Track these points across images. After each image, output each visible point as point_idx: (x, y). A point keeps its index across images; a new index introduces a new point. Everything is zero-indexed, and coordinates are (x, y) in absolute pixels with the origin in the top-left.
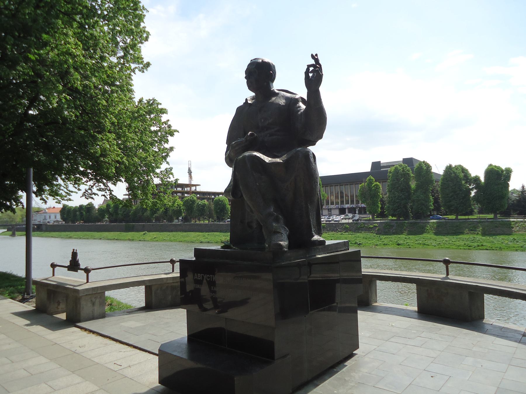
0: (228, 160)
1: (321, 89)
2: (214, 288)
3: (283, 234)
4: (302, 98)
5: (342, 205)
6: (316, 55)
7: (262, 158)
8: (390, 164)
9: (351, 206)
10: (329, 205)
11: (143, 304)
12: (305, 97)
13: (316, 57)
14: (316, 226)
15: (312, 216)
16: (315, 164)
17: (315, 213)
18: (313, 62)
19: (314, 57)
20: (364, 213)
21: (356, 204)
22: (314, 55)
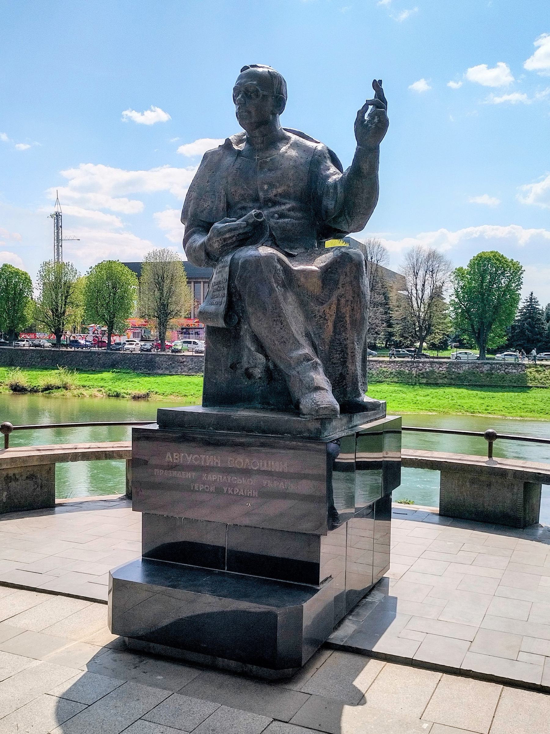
2: (207, 477)
6: (380, 81)
19: (377, 85)
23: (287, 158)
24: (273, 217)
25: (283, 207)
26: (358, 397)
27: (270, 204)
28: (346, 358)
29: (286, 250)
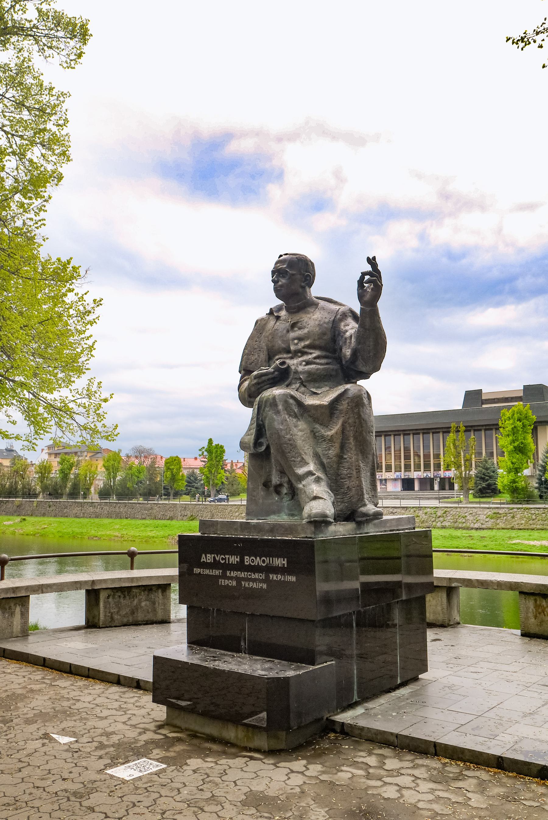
1: (379, 304)
2: (230, 573)
5: (407, 473)
6: (374, 258)
8: (507, 396)
9: (425, 475)
10: (401, 471)
11: (83, 623)
12: (358, 311)
16: (371, 407)
18: (369, 268)
19: (372, 261)
20: (450, 489)
21: (434, 470)
22: (371, 258)
24: (301, 364)
25: (310, 356)
26: (49, 472)
29: (312, 390)
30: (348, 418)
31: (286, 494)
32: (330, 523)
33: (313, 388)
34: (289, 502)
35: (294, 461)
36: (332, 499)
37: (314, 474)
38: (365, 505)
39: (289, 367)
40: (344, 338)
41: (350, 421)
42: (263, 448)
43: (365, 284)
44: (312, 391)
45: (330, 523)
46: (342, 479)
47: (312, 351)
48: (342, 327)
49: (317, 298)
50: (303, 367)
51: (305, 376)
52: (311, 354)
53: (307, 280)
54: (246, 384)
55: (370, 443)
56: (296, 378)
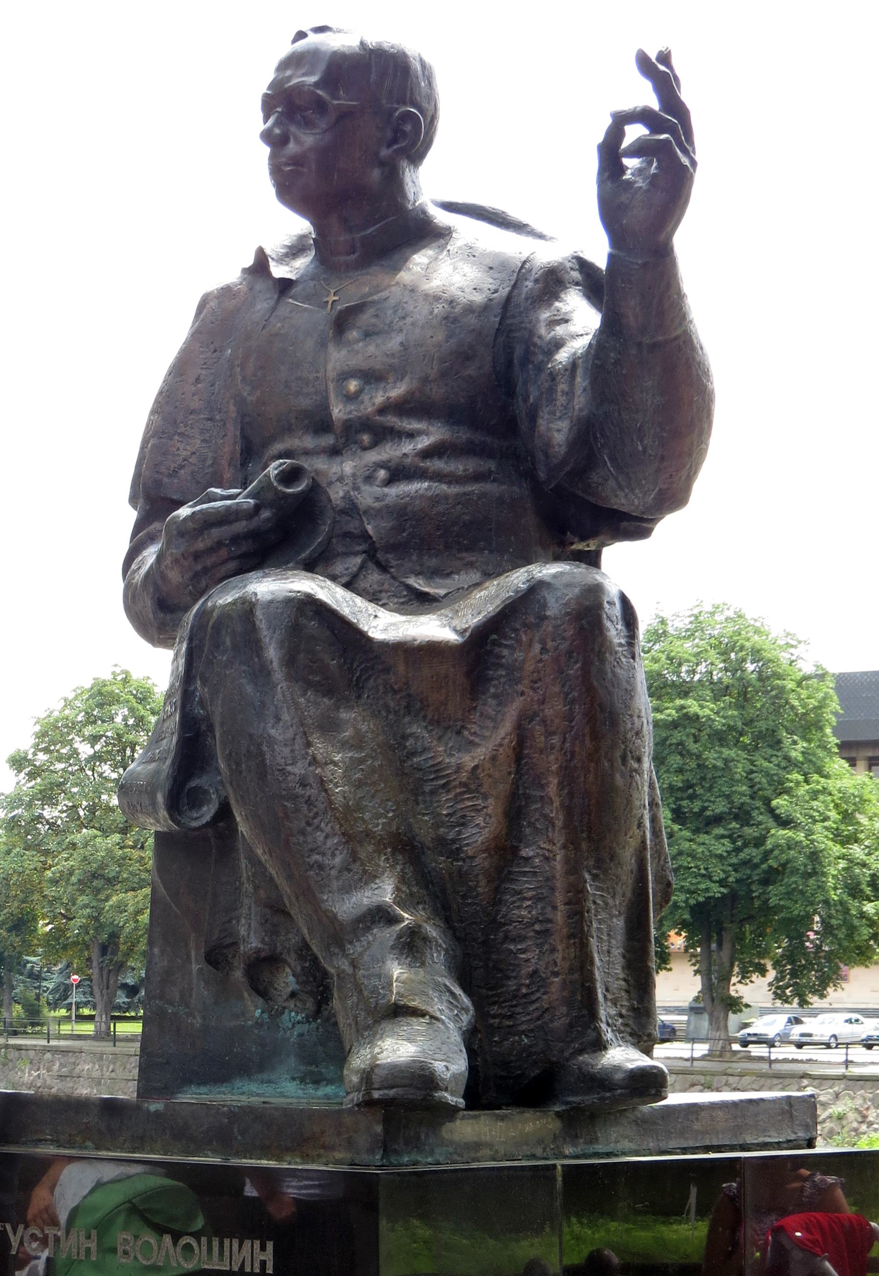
0: (147, 604)
3: (443, 1023)
4: (583, 265)
6: (665, 58)
7: (345, 611)
13: (662, 68)
14: (623, 994)
15: (605, 938)
17: (619, 923)
22: (653, 57)
23: (427, 295)
24: (369, 479)
25: (408, 448)
27: (366, 438)
28: (550, 921)
30: (542, 702)
31: (293, 995)
32: (451, 1112)
33: (418, 574)
34: (306, 1027)
35: (321, 867)
36: (465, 1018)
37: (397, 920)
38: (600, 1046)
39: (315, 488)
40: (544, 376)
41: (548, 712)
42: (208, 812)
43: (626, 162)
44: (409, 588)
45: (451, 1112)
46: (513, 940)
47: (414, 425)
48: (542, 331)
49: (450, 207)
50: (377, 490)
51: (386, 524)
52: (411, 435)
53: (404, 134)
54: (150, 555)
55: (629, 801)
56: (347, 535)
